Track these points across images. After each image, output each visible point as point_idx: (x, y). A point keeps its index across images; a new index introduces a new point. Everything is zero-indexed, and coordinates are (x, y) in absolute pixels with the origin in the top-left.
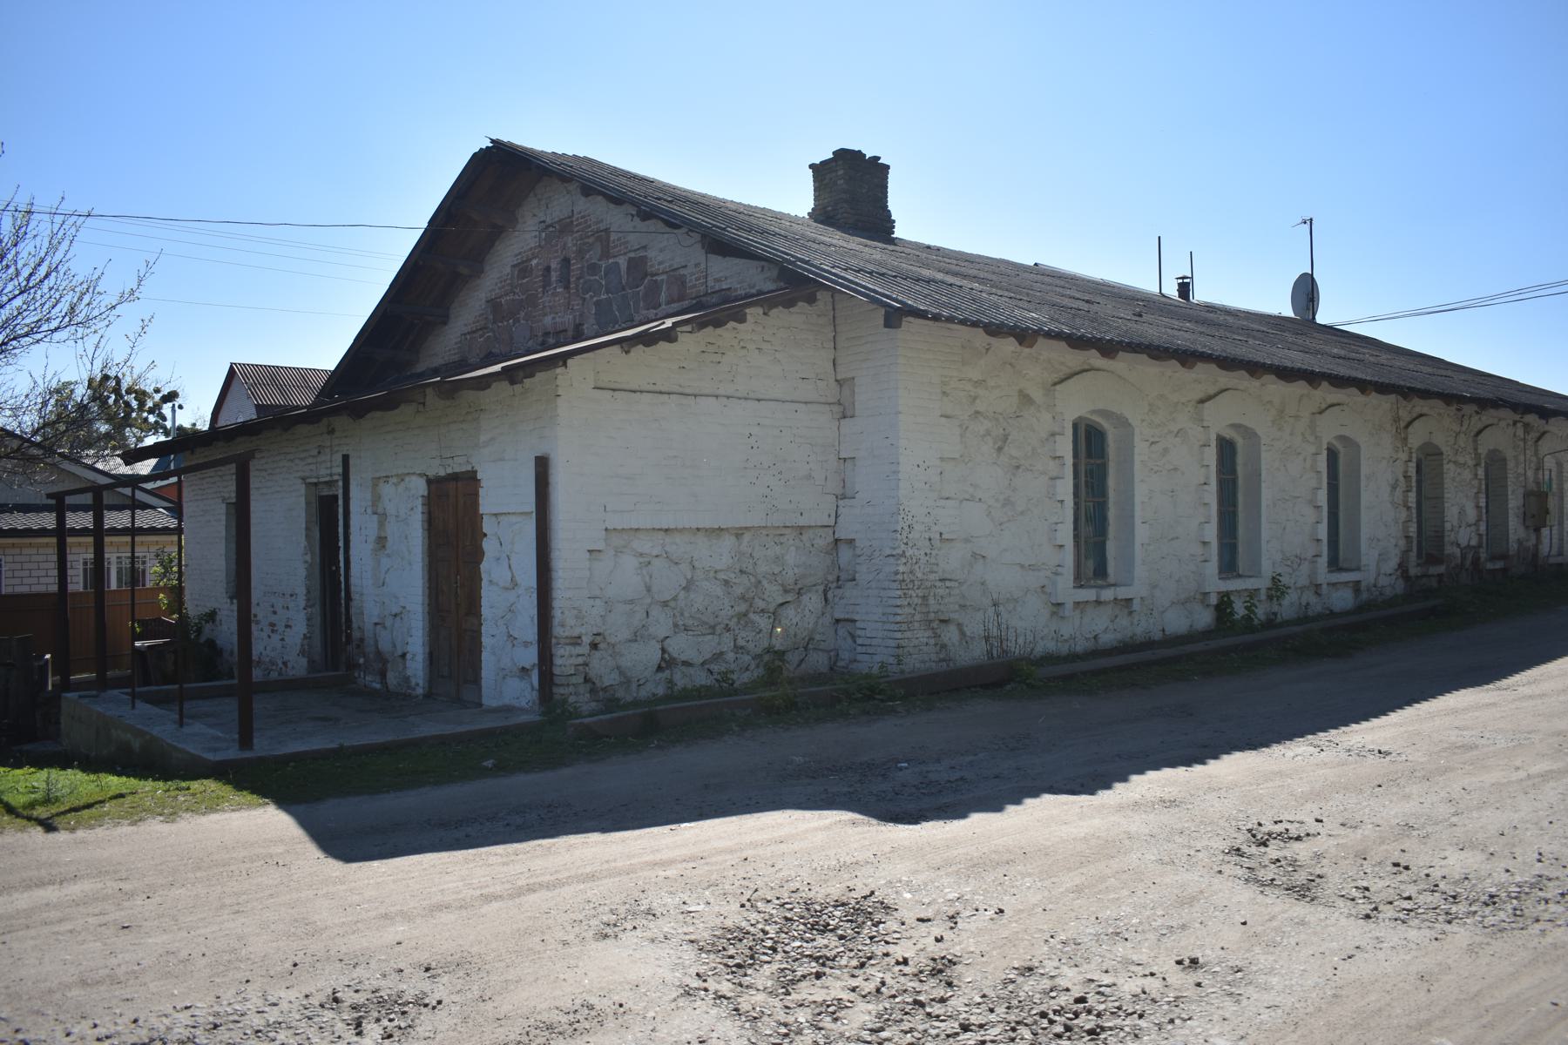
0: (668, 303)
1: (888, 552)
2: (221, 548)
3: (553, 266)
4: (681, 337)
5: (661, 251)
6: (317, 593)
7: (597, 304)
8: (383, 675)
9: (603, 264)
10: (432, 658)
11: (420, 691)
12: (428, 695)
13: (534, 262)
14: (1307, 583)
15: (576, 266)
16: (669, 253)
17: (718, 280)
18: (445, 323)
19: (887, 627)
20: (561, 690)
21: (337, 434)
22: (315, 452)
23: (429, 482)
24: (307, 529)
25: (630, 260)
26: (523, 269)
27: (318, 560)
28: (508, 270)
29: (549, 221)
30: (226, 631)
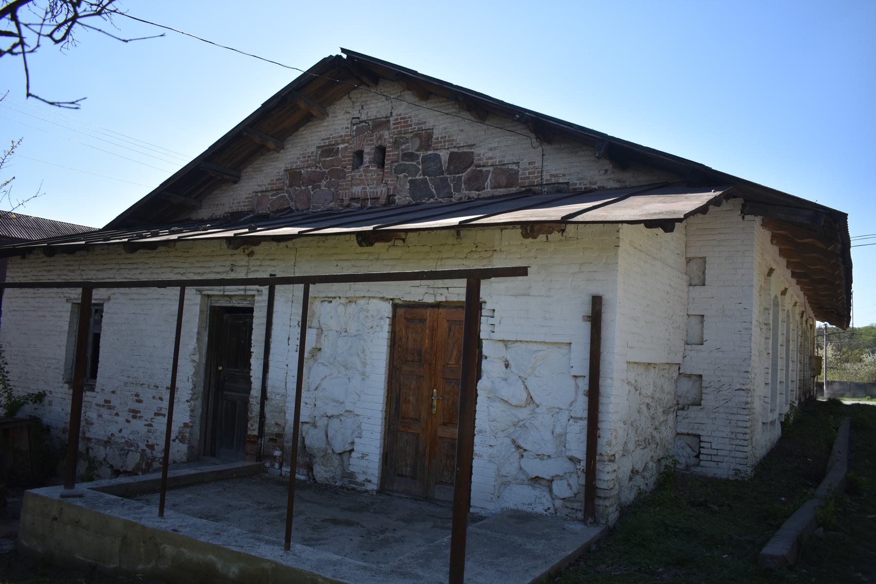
0: (494, 187)
1: (738, 387)
2: (63, 340)
3: (367, 150)
4: (710, 210)
5: (491, 149)
6: (200, 389)
7: (411, 182)
8: (310, 468)
9: (421, 154)
10: (386, 458)
11: (373, 487)
12: (381, 491)
13: (341, 146)
14: (649, 394)
15: (391, 154)
16: (495, 148)
17: (551, 176)
18: (235, 182)
19: (737, 442)
20: (601, 502)
21: (255, 257)
22: (228, 269)
23: (395, 307)
24: (199, 333)
25: (452, 154)
26: (328, 150)
27: (204, 361)
28: (314, 149)
29: (364, 117)
30: (58, 408)
